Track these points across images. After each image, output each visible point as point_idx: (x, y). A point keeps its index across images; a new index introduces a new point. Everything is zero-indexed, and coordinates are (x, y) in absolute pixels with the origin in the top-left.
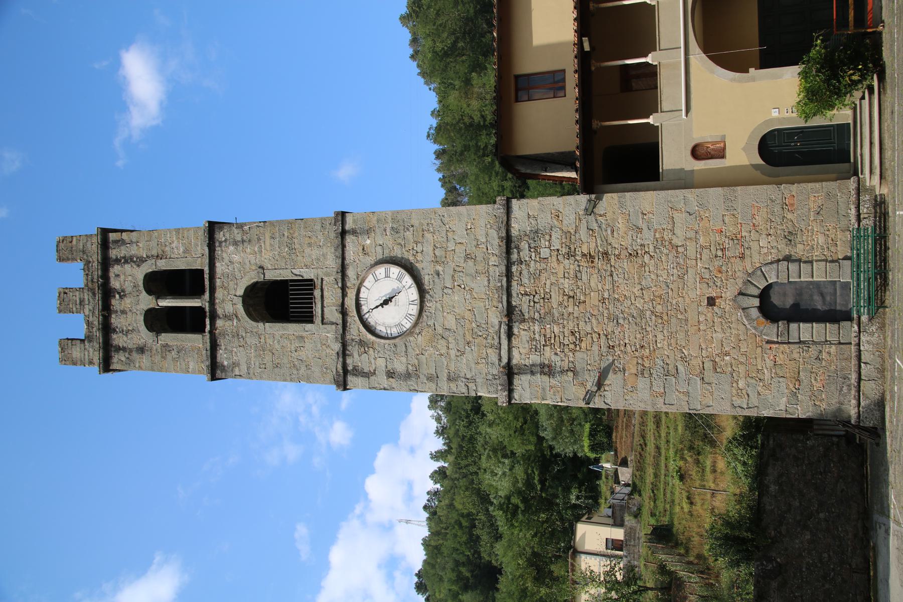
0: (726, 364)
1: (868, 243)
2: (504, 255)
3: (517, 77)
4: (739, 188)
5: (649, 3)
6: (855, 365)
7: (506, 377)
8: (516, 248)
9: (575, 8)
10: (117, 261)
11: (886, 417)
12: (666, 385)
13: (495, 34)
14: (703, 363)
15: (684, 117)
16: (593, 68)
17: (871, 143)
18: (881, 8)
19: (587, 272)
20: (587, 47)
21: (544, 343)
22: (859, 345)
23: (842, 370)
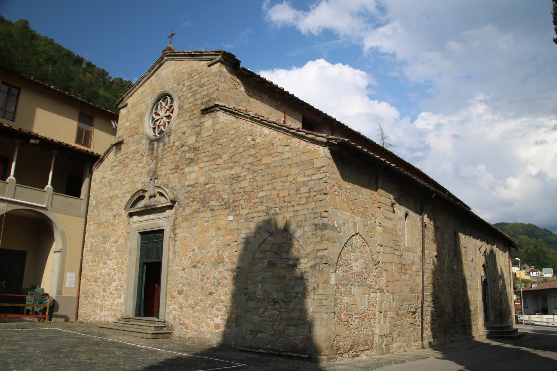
3: (19, 90)
5: (8, 178)
9: (60, 142)
11: (544, 288)
13: (52, 87)
16: (16, 140)
18: (6, 322)
20: (32, 141)
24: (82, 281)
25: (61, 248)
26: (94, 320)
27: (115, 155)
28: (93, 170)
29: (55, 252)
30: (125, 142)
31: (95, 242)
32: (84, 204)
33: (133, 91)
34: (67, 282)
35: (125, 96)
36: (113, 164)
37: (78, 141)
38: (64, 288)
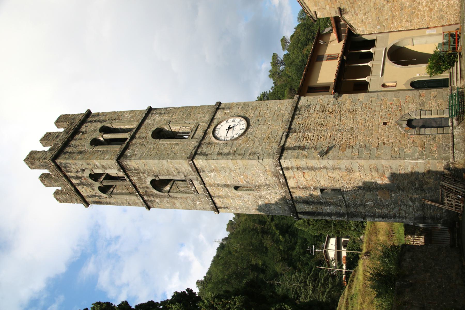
0: (390, 143)
1: (456, 101)
2: (293, 111)
4: (401, 92)
6: (451, 140)
7: (280, 150)
8: (299, 110)
12: (360, 151)
14: (379, 143)
15: (381, 76)
17: (457, 74)
21: (303, 139)
22: (453, 133)
23: (445, 143)
24: (432, 26)
25: (410, 39)
26: (458, 5)
27: (348, 13)
28: (356, 33)
29: (413, 45)
30: (339, 6)
31: (405, 18)
32: (378, 35)
33: (306, 8)
34: (432, 33)
35: (310, 14)
36: (353, 14)
37: (337, 59)
38: (437, 33)
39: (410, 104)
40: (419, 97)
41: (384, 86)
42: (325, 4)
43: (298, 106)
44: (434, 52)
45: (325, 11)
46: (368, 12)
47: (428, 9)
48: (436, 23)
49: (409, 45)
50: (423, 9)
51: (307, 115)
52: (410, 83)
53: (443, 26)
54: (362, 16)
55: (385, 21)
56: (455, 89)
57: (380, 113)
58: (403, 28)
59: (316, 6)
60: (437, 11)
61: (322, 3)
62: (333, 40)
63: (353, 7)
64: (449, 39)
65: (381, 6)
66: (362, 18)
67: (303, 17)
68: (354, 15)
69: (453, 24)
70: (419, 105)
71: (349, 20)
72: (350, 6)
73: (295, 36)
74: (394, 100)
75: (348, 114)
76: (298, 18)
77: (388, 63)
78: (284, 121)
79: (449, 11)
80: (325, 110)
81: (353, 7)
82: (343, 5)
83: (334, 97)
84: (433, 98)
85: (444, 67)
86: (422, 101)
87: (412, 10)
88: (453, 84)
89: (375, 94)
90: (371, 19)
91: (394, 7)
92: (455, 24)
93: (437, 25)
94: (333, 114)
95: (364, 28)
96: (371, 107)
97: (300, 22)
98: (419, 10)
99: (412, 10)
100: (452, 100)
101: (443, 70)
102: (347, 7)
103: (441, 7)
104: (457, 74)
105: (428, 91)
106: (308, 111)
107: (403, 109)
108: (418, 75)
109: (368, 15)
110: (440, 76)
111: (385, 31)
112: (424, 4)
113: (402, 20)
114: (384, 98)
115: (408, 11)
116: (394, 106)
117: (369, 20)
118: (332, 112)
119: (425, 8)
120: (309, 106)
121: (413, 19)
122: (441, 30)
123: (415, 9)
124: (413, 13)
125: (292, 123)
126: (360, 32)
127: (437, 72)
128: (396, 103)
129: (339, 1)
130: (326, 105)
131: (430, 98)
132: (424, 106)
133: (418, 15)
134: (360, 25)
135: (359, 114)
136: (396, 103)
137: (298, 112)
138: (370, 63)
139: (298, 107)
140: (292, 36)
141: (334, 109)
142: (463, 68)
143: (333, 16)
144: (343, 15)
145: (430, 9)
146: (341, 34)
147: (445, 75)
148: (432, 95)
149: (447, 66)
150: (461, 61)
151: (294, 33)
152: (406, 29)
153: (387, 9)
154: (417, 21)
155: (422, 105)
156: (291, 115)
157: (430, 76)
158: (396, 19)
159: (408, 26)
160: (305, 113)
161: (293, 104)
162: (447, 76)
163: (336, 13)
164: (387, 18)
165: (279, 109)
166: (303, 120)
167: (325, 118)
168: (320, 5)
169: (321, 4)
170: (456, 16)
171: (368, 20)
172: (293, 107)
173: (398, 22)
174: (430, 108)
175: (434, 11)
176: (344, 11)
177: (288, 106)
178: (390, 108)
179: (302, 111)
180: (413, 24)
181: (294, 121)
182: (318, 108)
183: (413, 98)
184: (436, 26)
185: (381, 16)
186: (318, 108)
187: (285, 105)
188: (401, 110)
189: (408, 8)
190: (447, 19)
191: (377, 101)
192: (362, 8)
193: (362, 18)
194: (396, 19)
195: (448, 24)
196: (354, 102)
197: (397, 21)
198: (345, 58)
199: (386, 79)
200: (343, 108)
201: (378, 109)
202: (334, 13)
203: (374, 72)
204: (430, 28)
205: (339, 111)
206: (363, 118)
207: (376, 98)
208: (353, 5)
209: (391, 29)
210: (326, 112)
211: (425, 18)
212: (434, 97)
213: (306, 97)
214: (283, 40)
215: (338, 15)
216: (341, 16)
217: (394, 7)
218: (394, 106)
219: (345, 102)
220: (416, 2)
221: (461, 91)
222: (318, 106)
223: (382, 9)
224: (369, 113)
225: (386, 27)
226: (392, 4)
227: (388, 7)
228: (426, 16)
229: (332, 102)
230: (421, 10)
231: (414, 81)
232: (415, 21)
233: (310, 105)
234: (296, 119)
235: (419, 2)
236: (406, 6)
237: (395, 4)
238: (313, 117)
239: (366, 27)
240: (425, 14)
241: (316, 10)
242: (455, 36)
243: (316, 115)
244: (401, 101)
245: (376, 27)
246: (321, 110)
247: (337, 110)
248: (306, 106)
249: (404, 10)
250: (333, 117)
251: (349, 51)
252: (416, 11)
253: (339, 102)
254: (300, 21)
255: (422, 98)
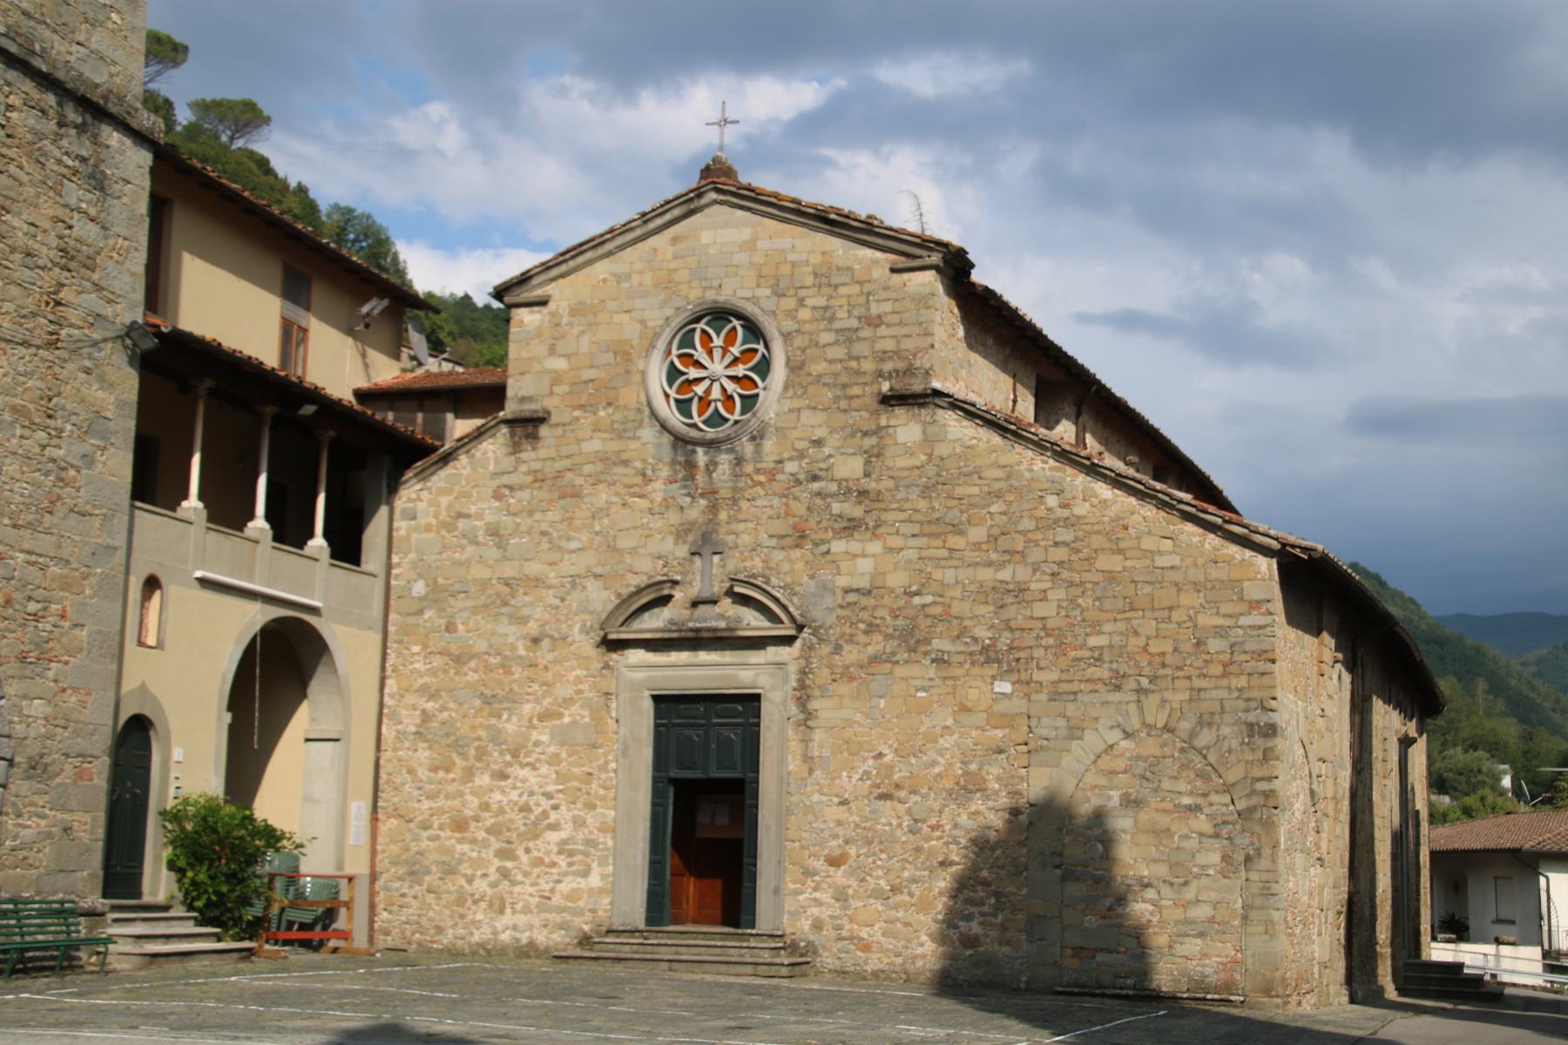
8: (84, 123)
10: (1251, 934)
15: (199, 574)
17: (168, 937)
19: (34, 284)
26: (460, 942)
28: (407, 481)
29: (308, 740)
30: (554, 419)
32: (379, 585)
33: (572, 264)
36: (505, 479)
39: (49, 710)
40: (79, 755)
41: (152, 584)
42: (576, 354)
43: (103, 127)
44: (283, 833)
45: (539, 349)
46: (501, 546)
47: (468, 813)
48: (392, 846)
49: (313, 720)
50: (472, 793)
51: (51, 164)
52: (147, 712)
53: (374, 877)
54: (490, 517)
55: (443, 622)
56: (90, 929)
57: (22, 551)
58: (392, 696)
59: (573, 312)
60: (449, 851)
61: (585, 340)
62: (366, 366)
63: (538, 479)
64: (312, 904)
65: (518, 609)
66: (479, 516)
67: (352, 236)
68: (498, 482)
69: (371, 922)
70: (37, 751)
71: (478, 454)
72: (547, 470)
73: (263, 178)
74: (77, 632)
75: (38, 384)
76: (350, 211)
77: (256, 616)
78: (32, 23)
79: (438, 904)
80: (72, 265)
81: (538, 479)
82: (558, 437)
83: (133, 326)
84: (62, 821)
85: (202, 877)
86: (57, 769)
87: (476, 743)
88: (116, 920)
89: (120, 540)
90: (464, 557)
91: (503, 666)
92: (371, 929)
93: (383, 851)
94: (47, 303)
95: (423, 521)
96: (60, 510)
97: (329, 216)
98: (469, 774)
99: (476, 743)
100: (42, 914)
101: (184, 875)
102: (543, 453)
103: (466, 869)
104: (168, 937)
105: (102, 801)
106: (76, 172)
107: (27, 672)
108: (177, 754)
109: (485, 544)
110: (157, 857)
111: (393, 616)
112: (497, 796)
113: (432, 697)
114: (93, 580)
115: (473, 727)
116: (49, 627)
117: (463, 548)
118: (58, 303)
119: (474, 802)
120: (99, 183)
121: (430, 748)
122: (357, 865)
123: (478, 758)
124: (462, 747)
125: (17, 69)
126: (410, 500)
127: (182, 846)
128: (64, 640)
129: (577, 419)
130: (96, 277)
131: (64, 809)
132: (29, 778)
133: (448, 770)
134: (444, 501)
135: (30, 445)
136: (64, 640)
137: (73, 115)
138: (262, 530)
139: (101, 121)
140: (263, 164)
141: (73, 315)
142: (194, 965)
143: (510, 382)
144: (505, 430)
145: (467, 823)
146: (391, 409)
147: (158, 882)
148: (78, 816)
149: (206, 892)
150: (225, 956)
151: (281, 175)
152: (385, 711)
153: (501, 635)
154: (420, 765)
155: (34, 768)
156: (60, 75)
157: (163, 813)
158: (445, 671)
159: (401, 723)
160: (67, 154)
161: (119, 99)
162: (155, 893)
163: (523, 400)
164: (456, 631)
165: (101, 17)
166: (29, 137)
167: (29, 261)
168: (576, 330)
169: (578, 336)
170: (408, 933)
171: (464, 542)
172: (106, 98)
173: (427, 679)
174: (14, 805)
175: (451, 837)
176: (528, 436)
177: (113, 70)
178: (39, 606)
179: (75, 139)
180: (407, 745)
181: (28, 86)
182: (85, 230)
183: (76, 722)
184: (379, 848)
185: (471, 603)
186: (85, 230)
187: (118, 55)
188: (22, 658)
189: (488, 727)
190: (403, 895)
191: (86, 544)
192: (524, 522)
193: (479, 516)
194: (445, 671)
195: (381, 899)
196: (95, 425)
197: (433, 672)
198: (309, 410)
199: (180, 596)
200: (70, 366)
201: (45, 543)
202: (521, 389)
203: (222, 542)
204: (374, 819)
205: (58, 340)
206: (8, 461)
207: (100, 541)
208: (549, 482)
209: (400, 642)
210: (57, 270)
211: (427, 798)
212: (67, 830)
213: (147, 177)
214: (249, 117)
215: (510, 409)
216: (506, 422)
217: (503, 666)
218: (49, 627)
219: (102, 379)
220: (509, 764)
221: (79, 959)
222: (93, 236)
223: (505, 610)
224: (30, 496)
225: (412, 620)
226: (520, 657)
227: (511, 639)
228: (434, 805)
229: (108, 311)
230: (470, 785)
231: (152, 733)
232: (418, 754)
233: (102, 189)
234: (36, 94)
235: (505, 777)
236: (500, 717)
237: (518, 672)
238: (38, 195)
239: (428, 528)
240: (447, 797)
241: (552, 306)
242: (325, 928)
243: (51, 212)
244: (66, 663)
245: (420, 576)
246: (72, 243)
247: (63, 332)
248: (102, 167)
249: (480, 710)
250: (30, 303)
251: (332, 433)
252: (468, 760)
253: (101, 350)
254: (335, 217)
255: (68, 768)
